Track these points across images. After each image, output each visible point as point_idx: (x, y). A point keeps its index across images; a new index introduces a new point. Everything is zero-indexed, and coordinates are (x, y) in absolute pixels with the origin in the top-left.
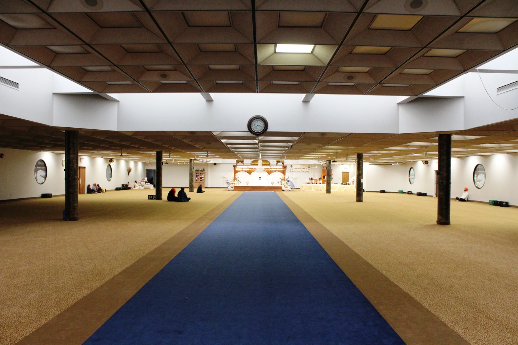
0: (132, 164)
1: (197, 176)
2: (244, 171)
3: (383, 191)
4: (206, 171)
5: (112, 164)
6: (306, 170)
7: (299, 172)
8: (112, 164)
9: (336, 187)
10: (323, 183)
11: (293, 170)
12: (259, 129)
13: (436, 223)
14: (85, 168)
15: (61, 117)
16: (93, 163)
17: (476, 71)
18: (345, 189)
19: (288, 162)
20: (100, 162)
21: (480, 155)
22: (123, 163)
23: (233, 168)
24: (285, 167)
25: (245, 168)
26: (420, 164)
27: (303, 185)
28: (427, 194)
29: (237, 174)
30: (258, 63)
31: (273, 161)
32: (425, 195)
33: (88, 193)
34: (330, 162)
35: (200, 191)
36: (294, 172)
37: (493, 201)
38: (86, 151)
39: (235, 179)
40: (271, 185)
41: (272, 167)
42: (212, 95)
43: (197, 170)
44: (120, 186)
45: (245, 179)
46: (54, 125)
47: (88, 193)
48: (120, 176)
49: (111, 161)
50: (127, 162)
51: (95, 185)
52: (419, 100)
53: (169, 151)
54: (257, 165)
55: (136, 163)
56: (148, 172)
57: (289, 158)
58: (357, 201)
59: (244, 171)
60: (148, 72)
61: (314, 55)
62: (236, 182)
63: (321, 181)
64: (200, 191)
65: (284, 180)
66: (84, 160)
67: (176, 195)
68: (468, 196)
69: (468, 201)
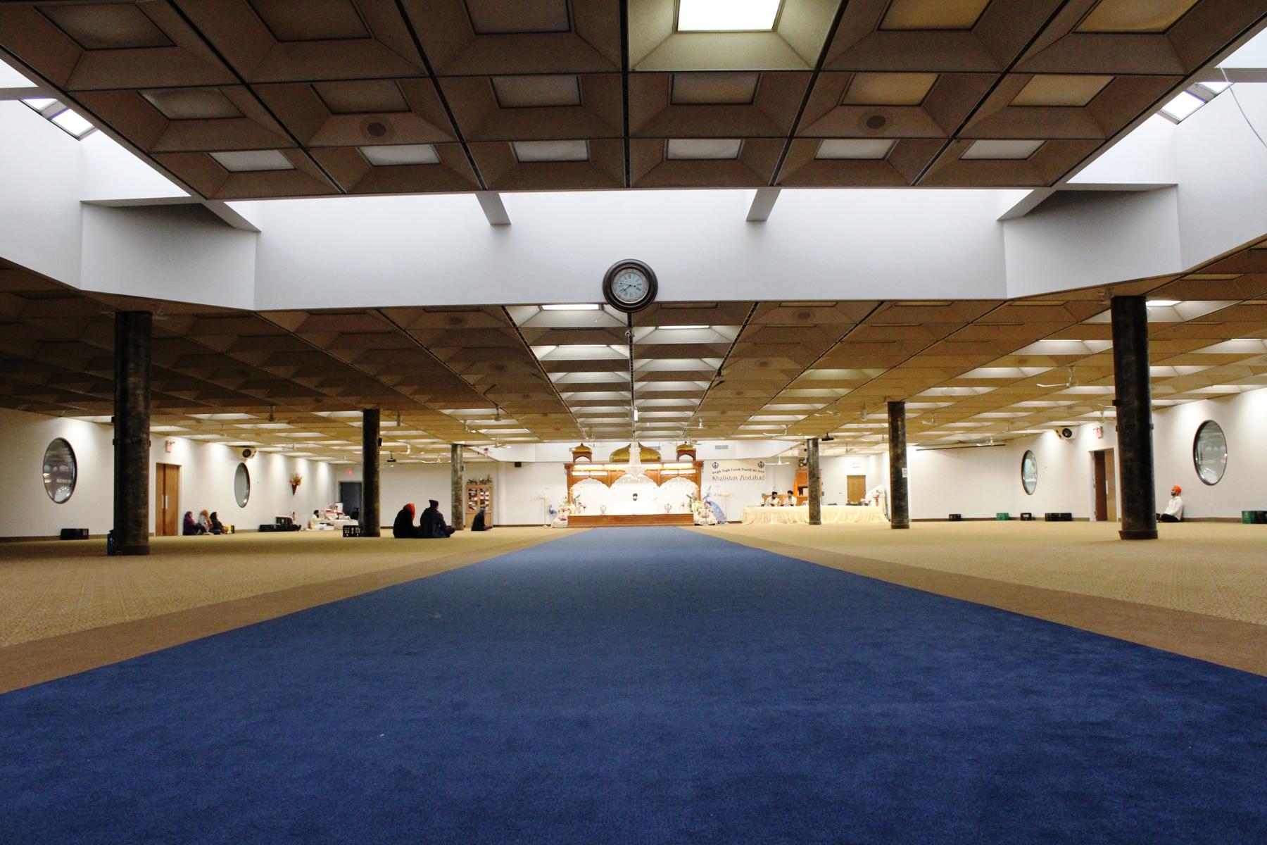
0: (302, 468)
1: (470, 496)
2: (594, 478)
3: (956, 518)
4: (495, 484)
5: (251, 463)
6: (753, 474)
7: (734, 478)
8: (251, 463)
9: (836, 513)
10: (800, 503)
11: (720, 475)
12: (635, 296)
13: (1118, 537)
14: (177, 467)
15: (103, 267)
16: (199, 459)
17: (1218, 76)
18: (856, 517)
19: (706, 448)
20: (219, 454)
21: (1211, 397)
22: (278, 462)
23: (563, 471)
24: (699, 465)
25: (597, 470)
26: (1051, 441)
27: (748, 510)
28: (1074, 516)
29: (575, 487)
30: (630, 67)
31: (668, 449)
32: (1067, 517)
33: (185, 533)
34: (816, 444)
35: (479, 524)
36: (723, 479)
37: (1251, 513)
38: (180, 411)
39: (570, 500)
40: (663, 512)
41: (666, 466)
42: (506, 198)
43: (471, 482)
44: (273, 522)
45: (596, 499)
46: (82, 288)
47: (185, 533)
48: (268, 499)
49: (247, 453)
50: (290, 460)
51: (204, 513)
52: (1061, 204)
53: (400, 407)
54: (627, 461)
55: (313, 464)
56: (346, 491)
57: (712, 431)
58: (894, 527)
59: (594, 478)
60: (334, 118)
61: (780, 36)
62: (572, 507)
63: (794, 500)
64: (479, 524)
65: (699, 498)
66: (174, 447)
67: (416, 522)
68: (1183, 509)
69: (1183, 520)
